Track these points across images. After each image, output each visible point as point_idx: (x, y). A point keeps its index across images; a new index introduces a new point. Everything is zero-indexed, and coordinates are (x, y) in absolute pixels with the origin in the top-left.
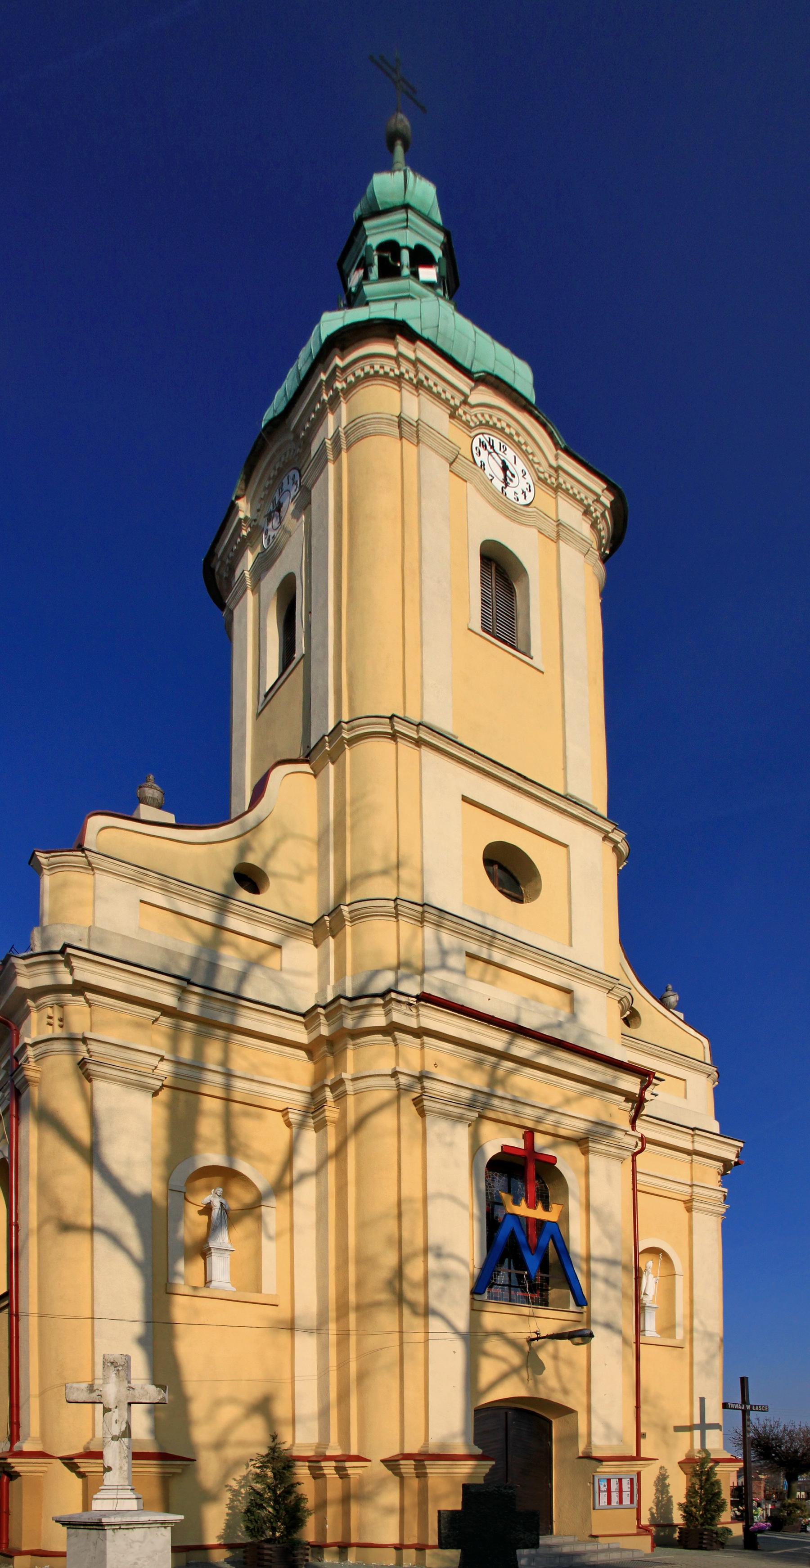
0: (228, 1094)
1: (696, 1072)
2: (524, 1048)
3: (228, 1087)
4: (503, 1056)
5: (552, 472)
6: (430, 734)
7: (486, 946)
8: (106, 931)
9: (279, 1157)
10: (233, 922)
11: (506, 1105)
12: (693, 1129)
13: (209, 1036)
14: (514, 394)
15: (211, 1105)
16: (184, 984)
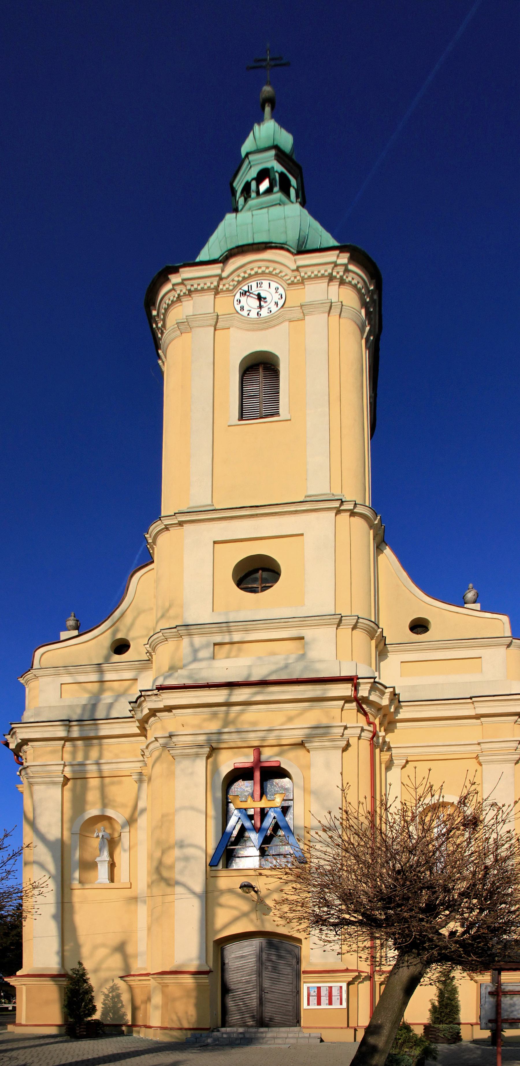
1: (492, 647)
2: (242, 695)
3: (100, 771)
4: (228, 704)
5: (296, 273)
6: (183, 516)
8: (40, 707)
9: (131, 804)
10: (108, 676)
11: (234, 736)
12: (471, 698)
13: (91, 745)
14: (255, 246)
15: (94, 783)
16: (67, 723)
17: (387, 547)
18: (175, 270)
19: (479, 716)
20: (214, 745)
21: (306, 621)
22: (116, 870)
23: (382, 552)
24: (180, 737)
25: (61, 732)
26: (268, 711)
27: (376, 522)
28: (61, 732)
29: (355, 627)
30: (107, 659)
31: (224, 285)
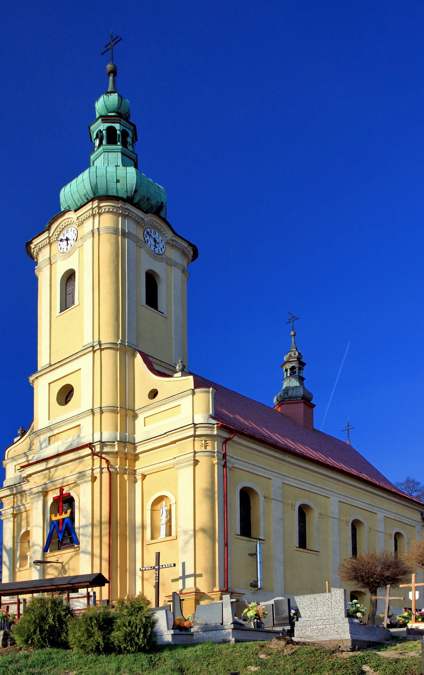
2: (52, 463)
3: (25, 508)
11: (51, 484)
12: (165, 433)
15: (24, 515)
18: (31, 242)
21: (78, 416)
24: (69, 477)
26: (64, 468)
27: (119, 347)
29: (102, 412)
31: (52, 239)
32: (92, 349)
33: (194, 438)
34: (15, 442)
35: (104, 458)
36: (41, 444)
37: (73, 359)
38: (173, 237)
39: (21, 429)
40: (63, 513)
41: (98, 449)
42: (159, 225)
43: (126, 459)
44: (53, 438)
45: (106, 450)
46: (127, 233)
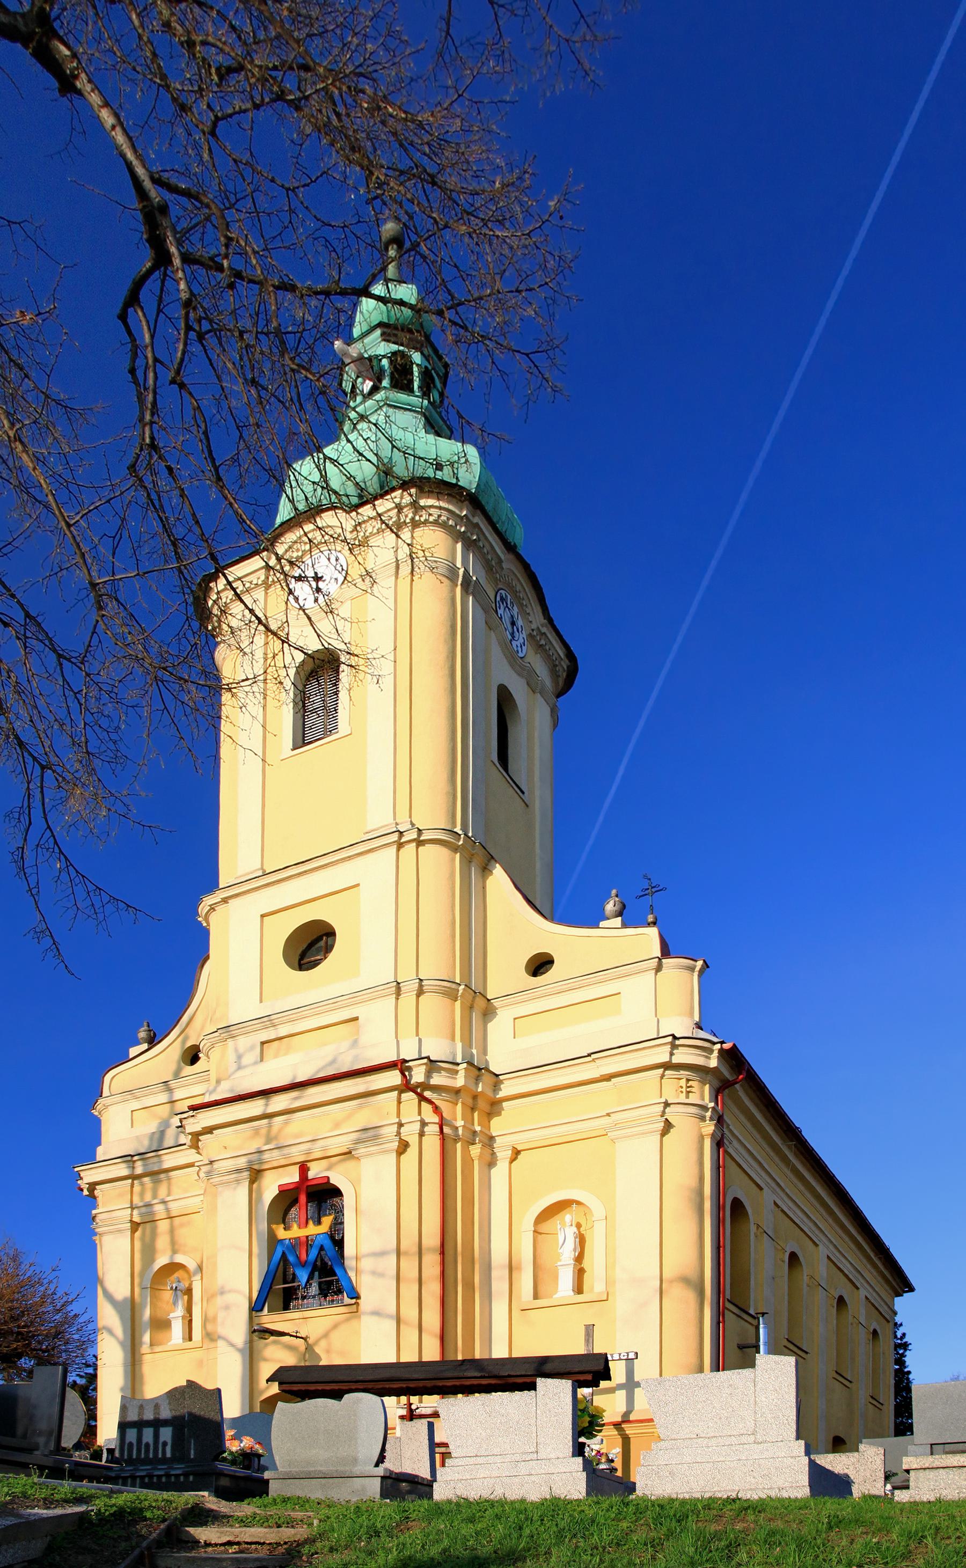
0: (169, 1214)
2: (280, 1102)
3: (168, 1210)
7: (272, 1028)
11: (276, 1153)
12: (589, 1055)
15: (163, 1226)
16: (129, 1158)
17: (498, 865)
19: (607, 1077)
20: (256, 1167)
21: (357, 996)
22: (586, 1276)
23: (491, 872)
25: (123, 1170)
27: (461, 842)
28: (123, 1170)
29: (420, 992)
30: (177, 1075)
32: (396, 839)
33: (664, 1072)
34: (131, 1057)
35: (429, 1101)
36: (240, 1057)
37: (337, 861)
38: (542, 626)
39: (146, 1028)
40: (311, 1222)
41: (418, 1076)
42: (522, 590)
43: (473, 1109)
44: (271, 1049)
45: (436, 1080)
46: (473, 583)
